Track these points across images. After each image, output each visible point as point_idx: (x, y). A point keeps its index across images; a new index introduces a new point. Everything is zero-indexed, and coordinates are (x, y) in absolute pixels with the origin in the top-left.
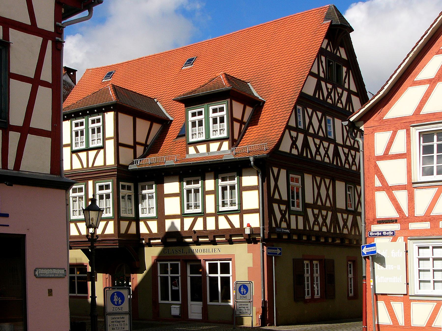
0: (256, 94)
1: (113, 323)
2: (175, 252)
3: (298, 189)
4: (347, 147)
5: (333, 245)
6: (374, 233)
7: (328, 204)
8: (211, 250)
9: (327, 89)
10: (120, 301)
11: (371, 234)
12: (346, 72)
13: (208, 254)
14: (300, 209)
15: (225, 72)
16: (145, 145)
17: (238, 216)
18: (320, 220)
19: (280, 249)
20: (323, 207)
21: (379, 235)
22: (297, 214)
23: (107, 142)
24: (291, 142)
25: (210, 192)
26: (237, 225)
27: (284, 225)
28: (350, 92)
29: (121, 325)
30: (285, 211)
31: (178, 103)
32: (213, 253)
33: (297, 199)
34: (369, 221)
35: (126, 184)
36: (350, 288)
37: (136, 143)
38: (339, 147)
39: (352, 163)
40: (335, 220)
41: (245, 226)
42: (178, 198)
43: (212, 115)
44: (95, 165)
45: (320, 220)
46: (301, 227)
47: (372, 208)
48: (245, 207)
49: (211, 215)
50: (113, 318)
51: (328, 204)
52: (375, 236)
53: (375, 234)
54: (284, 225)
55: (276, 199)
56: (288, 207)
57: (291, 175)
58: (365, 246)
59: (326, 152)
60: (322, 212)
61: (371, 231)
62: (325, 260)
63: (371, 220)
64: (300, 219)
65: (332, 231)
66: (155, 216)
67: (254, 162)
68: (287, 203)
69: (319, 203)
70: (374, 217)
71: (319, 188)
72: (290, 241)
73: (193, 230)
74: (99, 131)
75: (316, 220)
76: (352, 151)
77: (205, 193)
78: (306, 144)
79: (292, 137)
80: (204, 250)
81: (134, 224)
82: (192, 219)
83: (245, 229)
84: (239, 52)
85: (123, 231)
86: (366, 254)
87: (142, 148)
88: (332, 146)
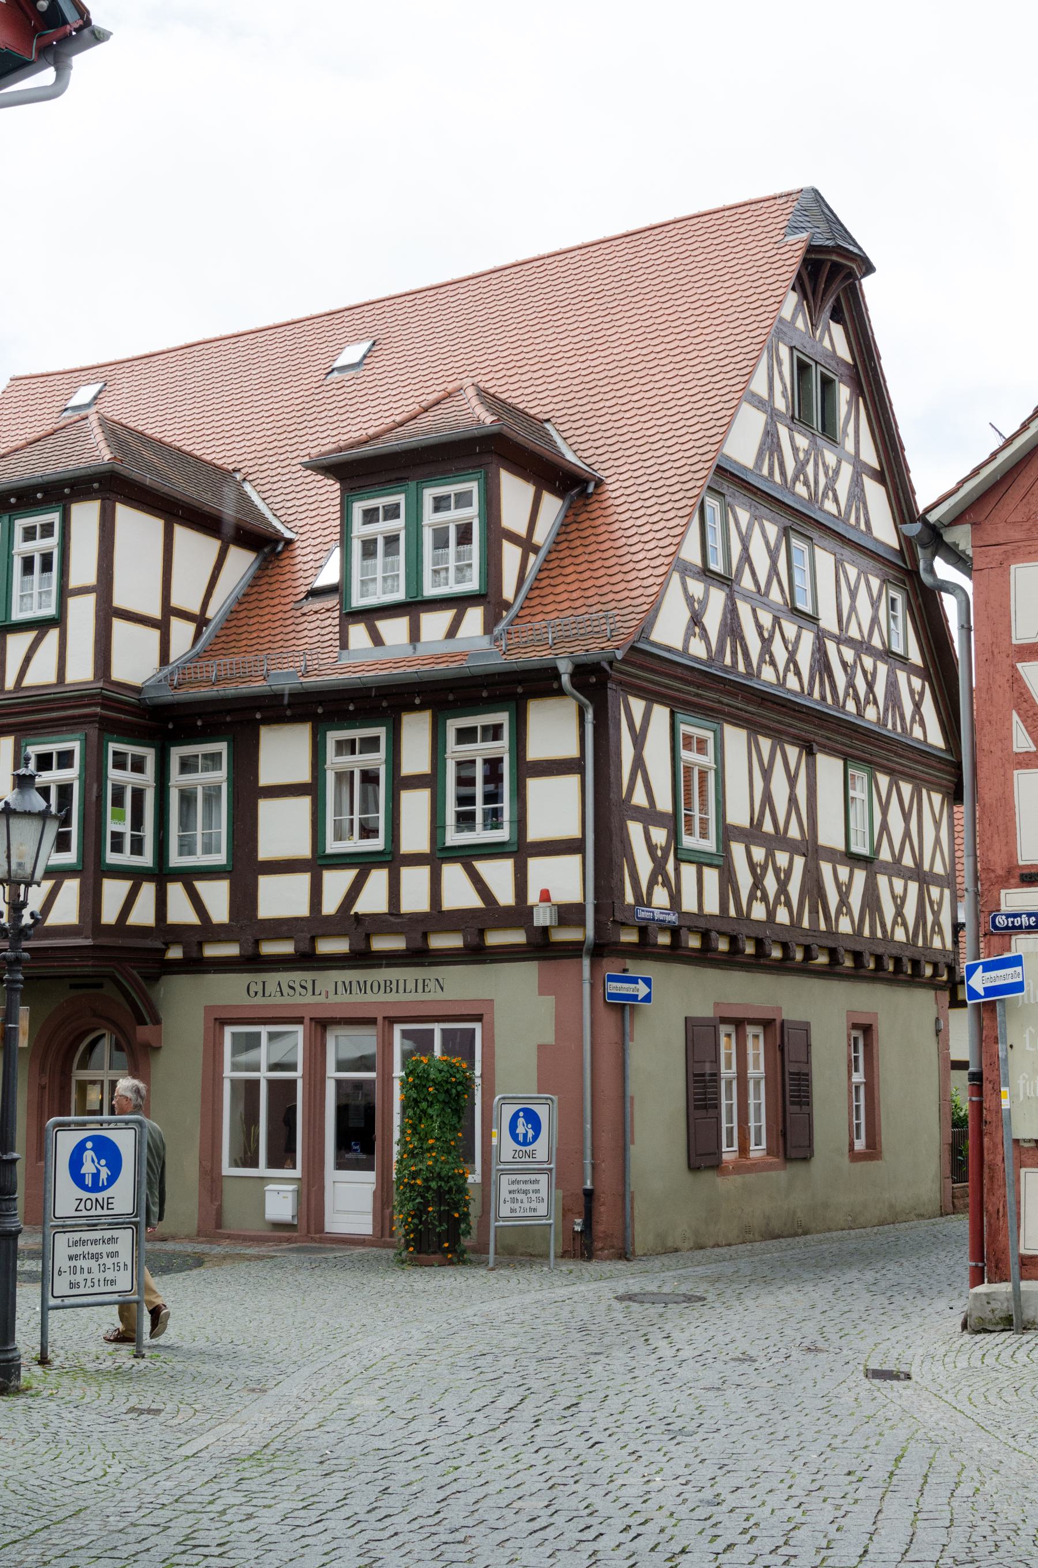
0: (570, 457)
1: (73, 1263)
2: (286, 990)
3: (703, 775)
4: (850, 642)
5: (806, 970)
6: (1010, 920)
7: (794, 832)
8: (410, 986)
9: (795, 449)
10: (105, 1173)
11: (1001, 921)
12: (849, 403)
13: (401, 997)
14: (710, 845)
15: (476, 380)
16: (201, 621)
17: (507, 866)
18: (770, 884)
19: (648, 982)
20: (778, 841)
21: (1029, 927)
22: (701, 861)
23: (72, 602)
24: (686, 615)
25: (416, 782)
26: (506, 897)
27: (661, 897)
28: (860, 468)
29: (102, 1268)
30: (666, 851)
31: (320, 477)
32: (420, 996)
33: (701, 811)
34: (992, 875)
35: (131, 750)
36: (855, 1122)
37: (169, 611)
38: (827, 641)
39: (867, 699)
40: (813, 887)
41: (533, 897)
42: (304, 803)
43: (430, 518)
44: (27, 682)
45: (770, 884)
46: (712, 906)
47: (1001, 828)
48: (535, 833)
49: (415, 860)
50: (75, 1243)
51: (794, 832)
52: (1014, 927)
53: (1013, 922)
54: (661, 897)
55: (638, 808)
56: (674, 836)
57: (683, 729)
58: (979, 964)
59: (792, 659)
60: (777, 858)
61: (999, 910)
62: (783, 1023)
63: (1000, 872)
64: (711, 876)
65: (806, 924)
66: (224, 862)
67: (572, 676)
68: (673, 823)
69: (768, 827)
70: (1009, 862)
71: (767, 774)
72: (675, 953)
73: (352, 913)
74: (47, 567)
75: (758, 883)
76: (864, 657)
77: (399, 783)
78: (732, 627)
79: (690, 599)
80: (388, 983)
81: (148, 891)
82: (349, 876)
83: (535, 910)
84: (513, 326)
85: (109, 915)
86: (982, 994)
87: (191, 628)
88: (808, 638)
